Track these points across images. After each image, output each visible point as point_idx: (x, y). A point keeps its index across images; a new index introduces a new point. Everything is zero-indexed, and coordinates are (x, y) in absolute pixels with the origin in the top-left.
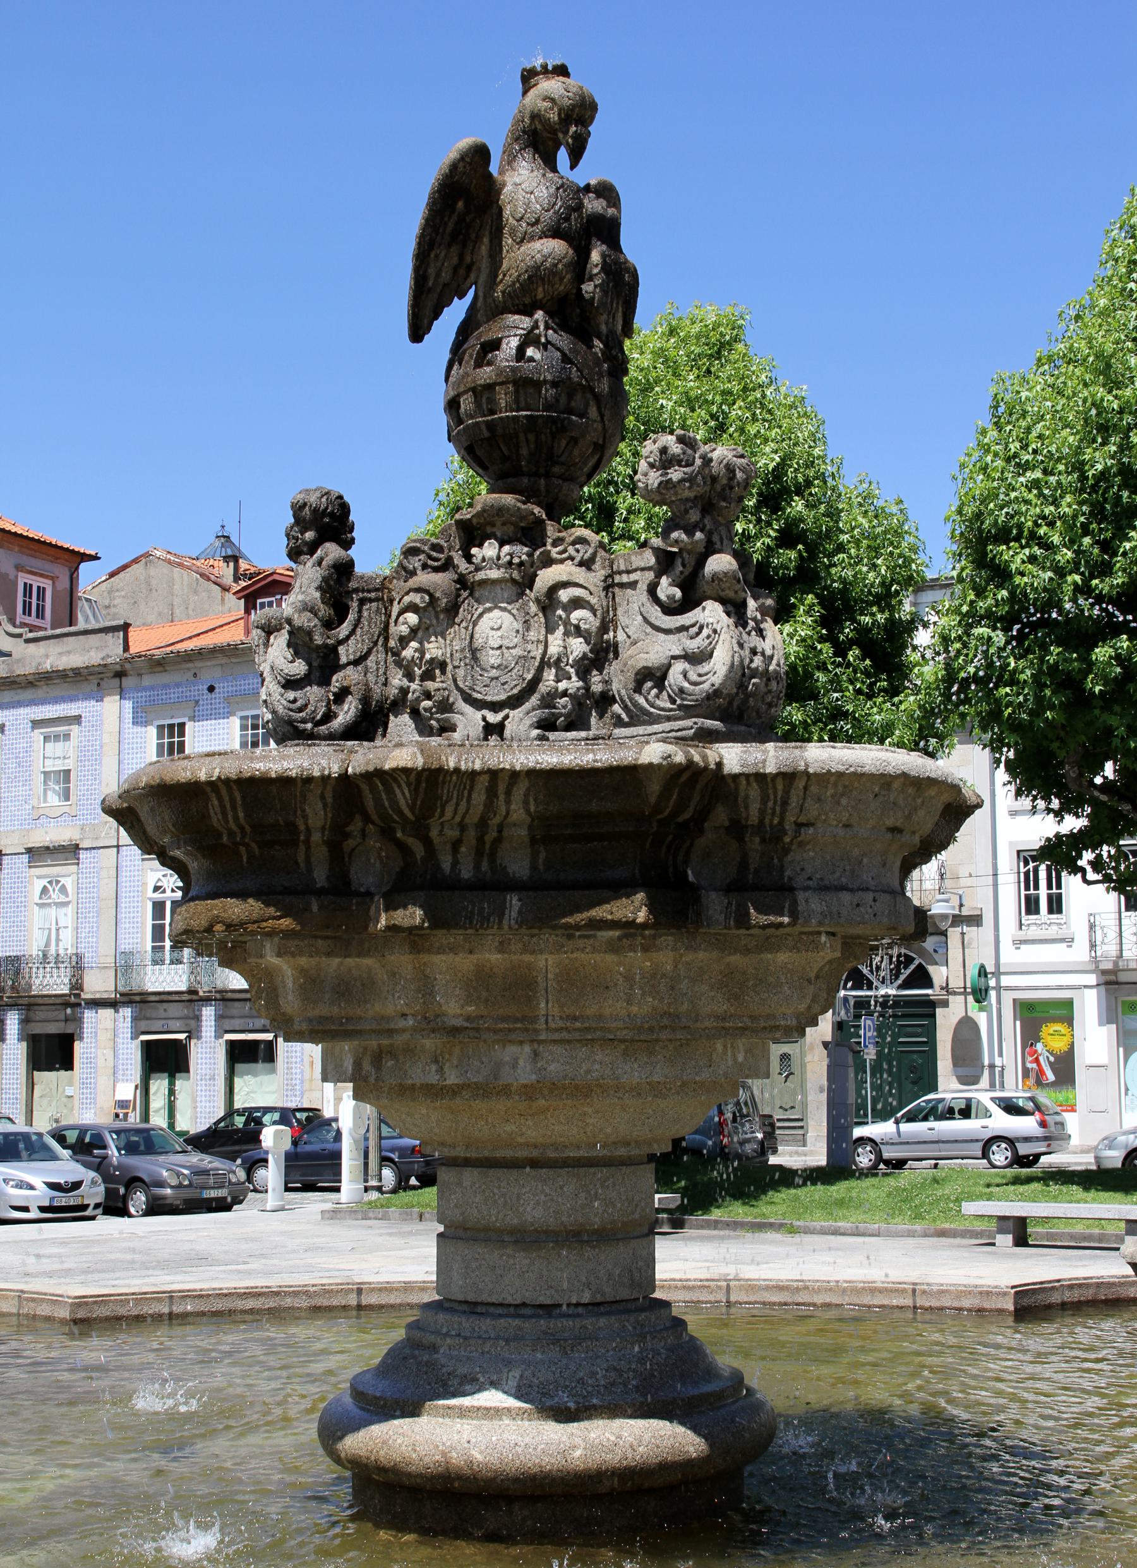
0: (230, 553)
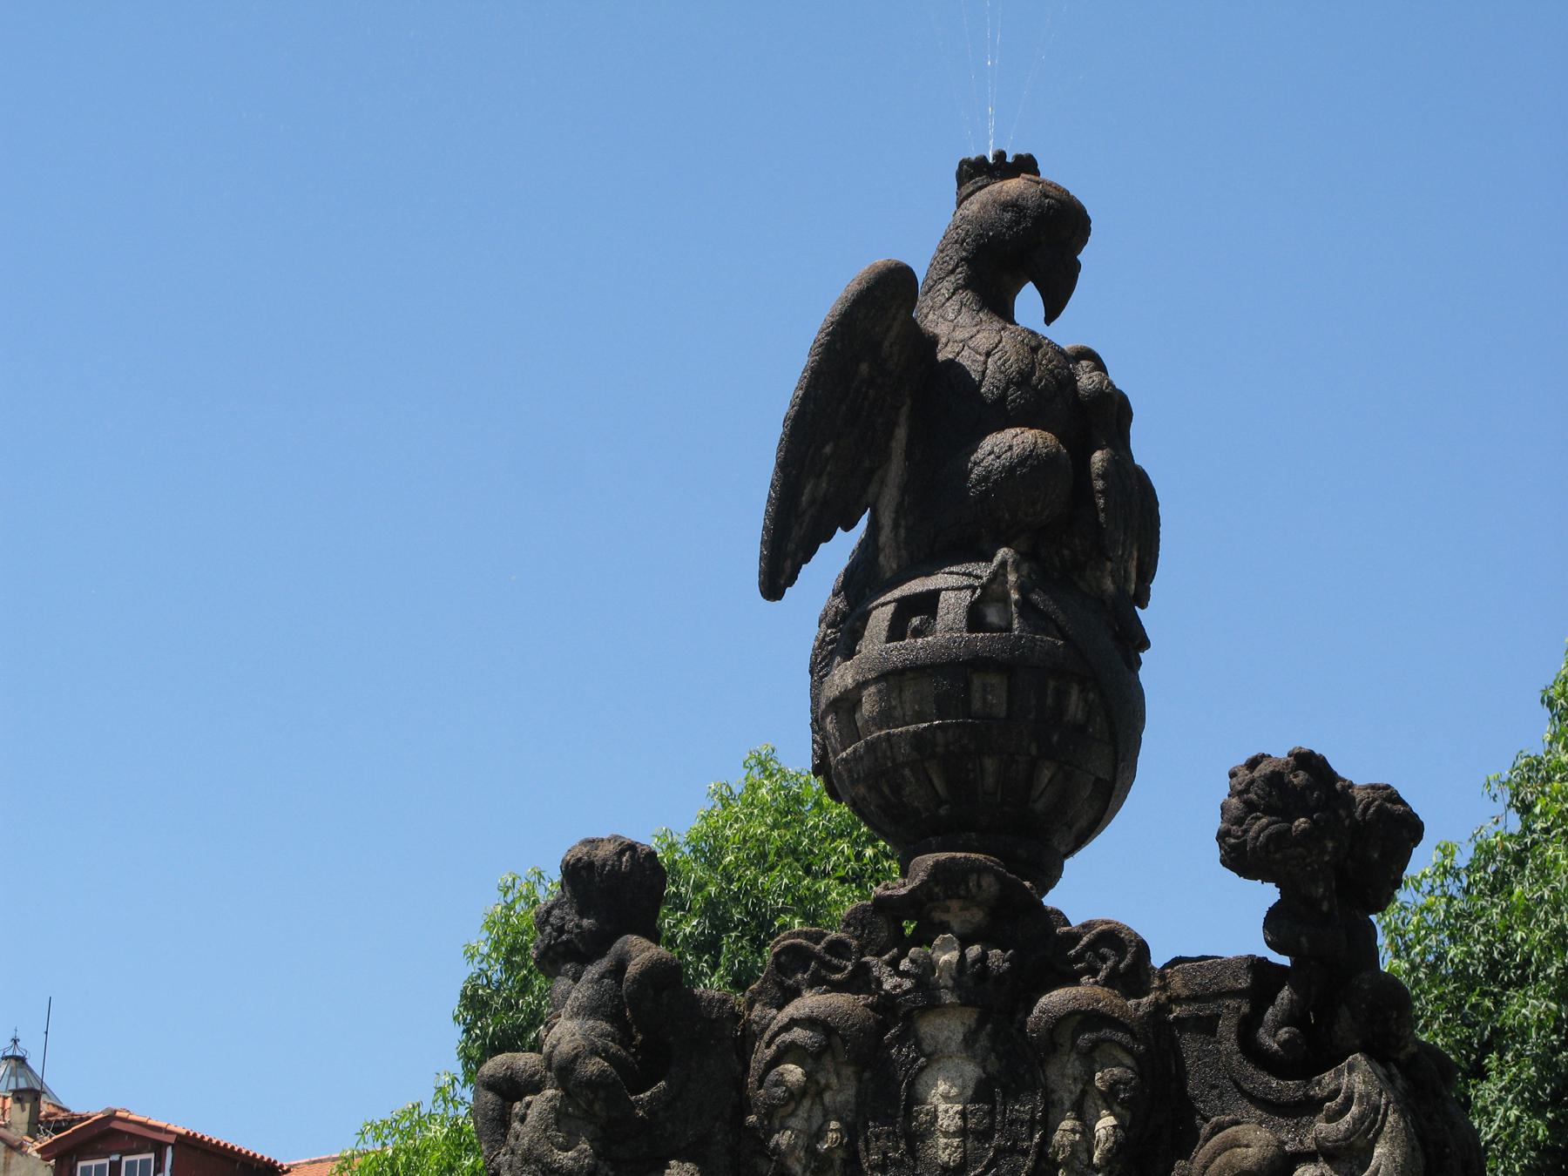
0: (23, 1084)
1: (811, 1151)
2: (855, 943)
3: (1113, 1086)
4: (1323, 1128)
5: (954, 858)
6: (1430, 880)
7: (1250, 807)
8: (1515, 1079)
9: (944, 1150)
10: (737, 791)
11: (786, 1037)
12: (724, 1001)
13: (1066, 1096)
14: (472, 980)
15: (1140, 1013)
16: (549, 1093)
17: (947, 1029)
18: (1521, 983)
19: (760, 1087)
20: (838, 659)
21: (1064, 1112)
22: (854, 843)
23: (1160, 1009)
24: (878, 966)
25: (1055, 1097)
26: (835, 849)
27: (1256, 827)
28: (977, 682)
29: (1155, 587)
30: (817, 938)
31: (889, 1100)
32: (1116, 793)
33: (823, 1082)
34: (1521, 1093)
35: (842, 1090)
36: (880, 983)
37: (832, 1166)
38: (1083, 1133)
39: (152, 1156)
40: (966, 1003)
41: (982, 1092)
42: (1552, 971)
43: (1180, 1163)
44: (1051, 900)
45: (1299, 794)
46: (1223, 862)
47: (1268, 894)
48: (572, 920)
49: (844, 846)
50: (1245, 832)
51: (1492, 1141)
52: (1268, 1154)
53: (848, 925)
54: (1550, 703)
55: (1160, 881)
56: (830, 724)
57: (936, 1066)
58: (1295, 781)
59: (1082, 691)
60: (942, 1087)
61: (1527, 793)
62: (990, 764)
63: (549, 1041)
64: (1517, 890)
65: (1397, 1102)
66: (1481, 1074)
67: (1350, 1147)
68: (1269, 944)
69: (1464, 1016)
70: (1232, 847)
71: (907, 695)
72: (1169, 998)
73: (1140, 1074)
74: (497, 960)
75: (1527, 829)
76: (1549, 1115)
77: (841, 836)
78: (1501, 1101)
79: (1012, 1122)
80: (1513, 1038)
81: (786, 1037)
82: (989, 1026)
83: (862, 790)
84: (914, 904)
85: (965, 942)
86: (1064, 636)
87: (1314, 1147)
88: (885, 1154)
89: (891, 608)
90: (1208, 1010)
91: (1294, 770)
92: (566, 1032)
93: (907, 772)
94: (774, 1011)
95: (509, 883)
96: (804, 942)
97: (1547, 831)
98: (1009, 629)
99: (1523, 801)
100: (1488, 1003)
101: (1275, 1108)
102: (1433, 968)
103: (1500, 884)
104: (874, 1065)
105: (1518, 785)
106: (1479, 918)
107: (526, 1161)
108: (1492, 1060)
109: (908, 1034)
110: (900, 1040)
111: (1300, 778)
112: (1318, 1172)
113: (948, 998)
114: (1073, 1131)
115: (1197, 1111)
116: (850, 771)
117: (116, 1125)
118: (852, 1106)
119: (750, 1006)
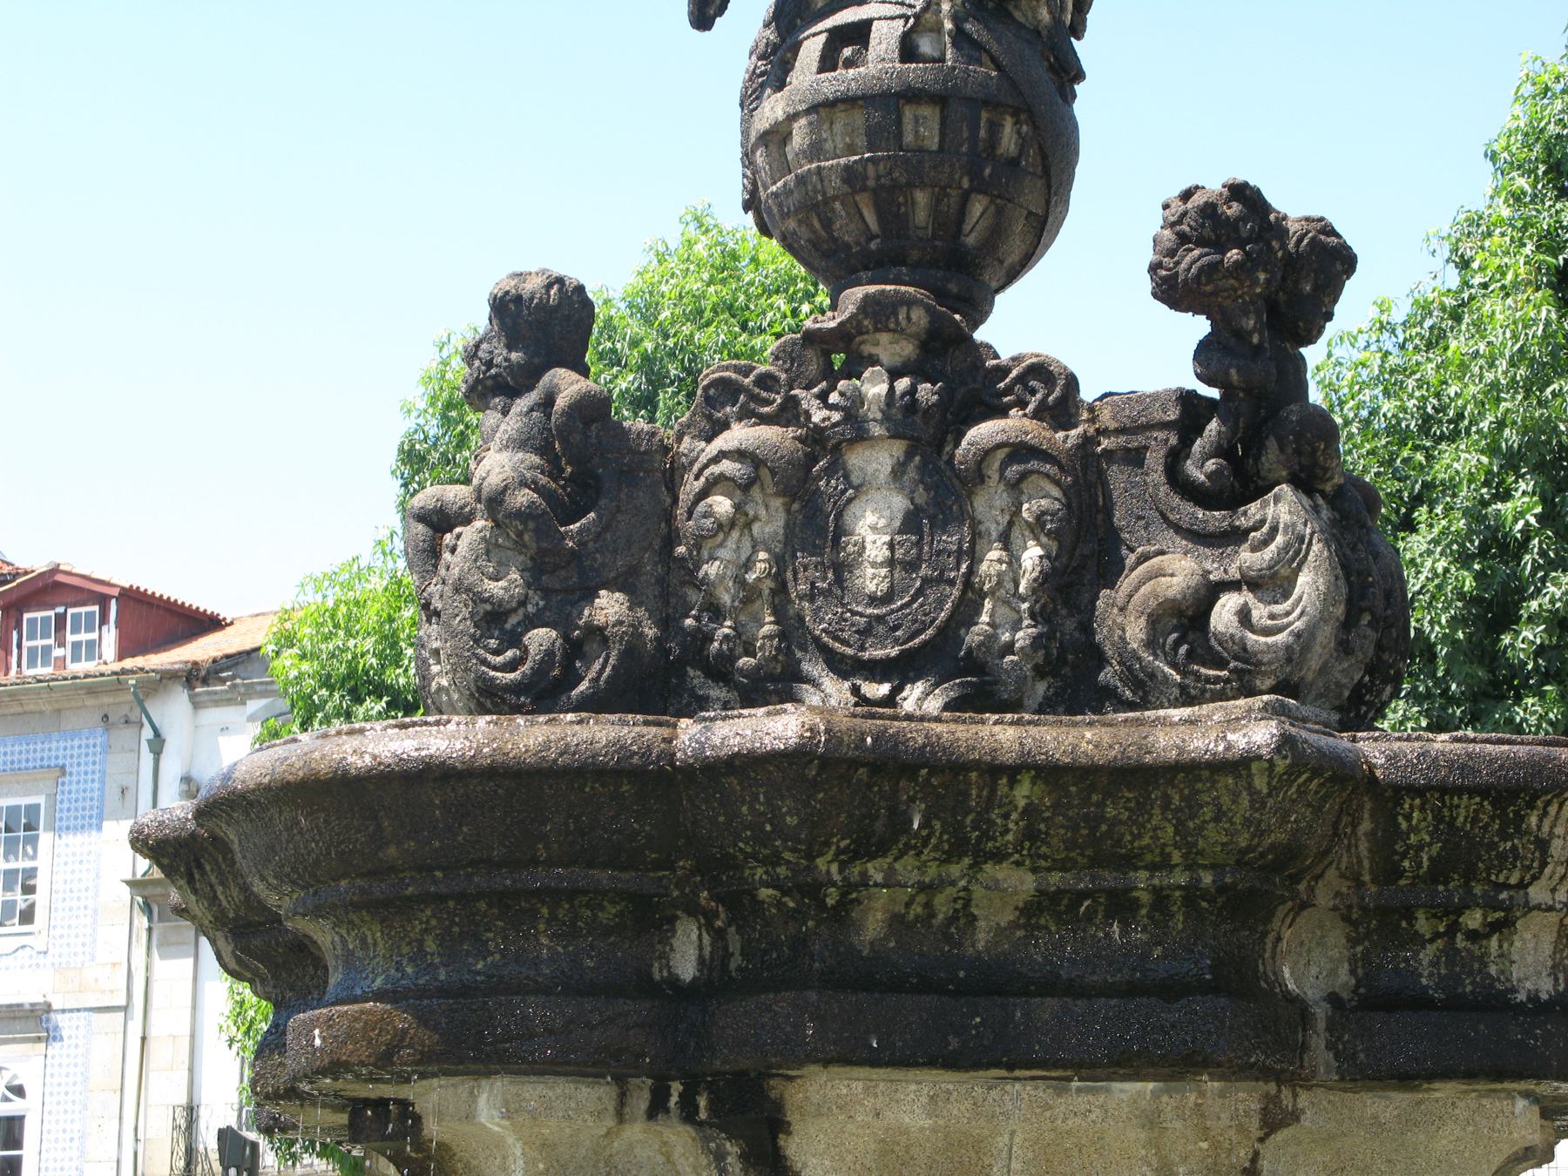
1: (740, 582)
2: (783, 376)
3: (1040, 517)
4: (1247, 558)
5: (883, 291)
6: (1366, 336)
7: (1183, 238)
8: (1444, 532)
9: (871, 579)
10: (672, 247)
11: (715, 469)
12: (653, 434)
13: (993, 527)
14: (410, 436)
15: (1069, 445)
16: (479, 524)
17: (876, 460)
18: (1453, 437)
19: (689, 519)
20: (768, 91)
21: (990, 543)
22: (791, 300)
23: (1087, 442)
24: (807, 399)
25: (982, 528)
26: (771, 306)
27: (1188, 259)
28: (908, 113)
29: (1091, 17)
30: (746, 371)
31: (816, 528)
32: (1048, 227)
33: (751, 513)
34: (1449, 545)
35: (771, 520)
36: (808, 415)
37: (761, 594)
38: (1010, 564)
39: (96, 608)
40: (894, 436)
41: (911, 523)
42: (1484, 425)
43: (1105, 592)
44: (980, 335)
45: (1233, 224)
46: (1155, 295)
47: (1199, 326)
48: (500, 354)
49: (780, 301)
50: (1177, 263)
51: (1419, 593)
52: (1193, 583)
53: (777, 358)
54: (1493, 157)
55: (1092, 315)
56: (760, 157)
57: (864, 498)
58: (1229, 212)
59: (1015, 124)
60: (870, 518)
61: (1467, 248)
62: (921, 197)
63: (479, 473)
64: (1453, 345)
65: (1322, 531)
66: (1409, 526)
67: (1274, 576)
68: (1199, 376)
69: (1396, 470)
70: (1164, 280)
71: (838, 127)
72: (1097, 430)
73: (1068, 506)
74: (433, 415)
75: (1466, 284)
76: (1477, 567)
77: (777, 292)
78: (1429, 553)
79: (939, 553)
80: (1443, 492)
81: (715, 469)
82: (917, 458)
83: (792, 224)
84: (844, 337)
85: (894, 374)
86: (999, 67)
87: (1238, 576)
88: (813, 584)
89: (823, 38)
90: (1136, 441)
91: (1228, 201)
92: (498, 465)
93: (837, 205)
94: (703, 444)
95: (445, 339)
96: (734, 376)
97: (1485, 286)
98: (942, 60)
99: (1462, 256)
100: (1420, 457)
101: (1201, 538)
102: (1367, 423)
103: (1435, 341)
104: (807, 495)
105: (1458, 240)
106: (1414, 373)
107: (457, 590)
108: (1421, 513)
109: (837, 467)
110: (829, 472)
111: (1234, 209)
112: (1242, 601)
113: (877, 430)
114: (1000, 561)
115: (1123, 541)
116: (780, 206)
117: (60, 578)
118: (781, 537)
119: (679, 439)
